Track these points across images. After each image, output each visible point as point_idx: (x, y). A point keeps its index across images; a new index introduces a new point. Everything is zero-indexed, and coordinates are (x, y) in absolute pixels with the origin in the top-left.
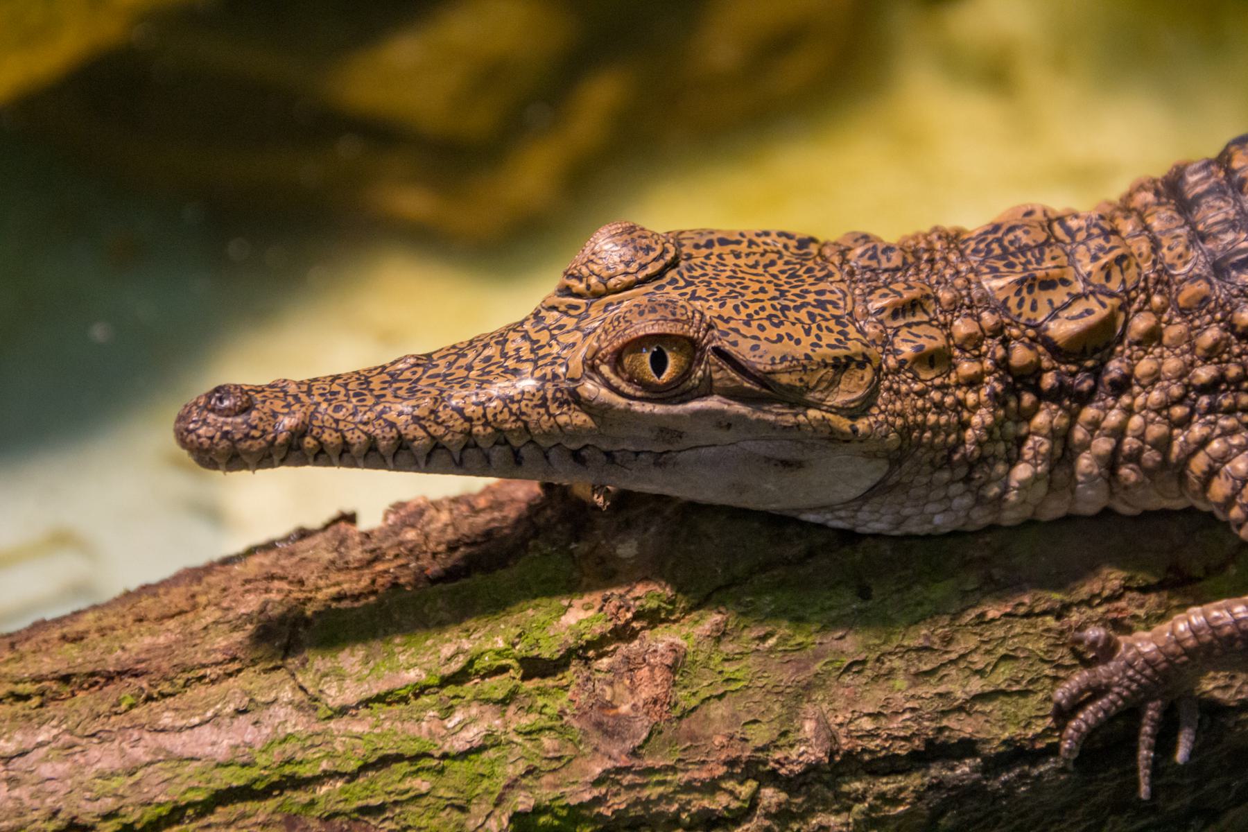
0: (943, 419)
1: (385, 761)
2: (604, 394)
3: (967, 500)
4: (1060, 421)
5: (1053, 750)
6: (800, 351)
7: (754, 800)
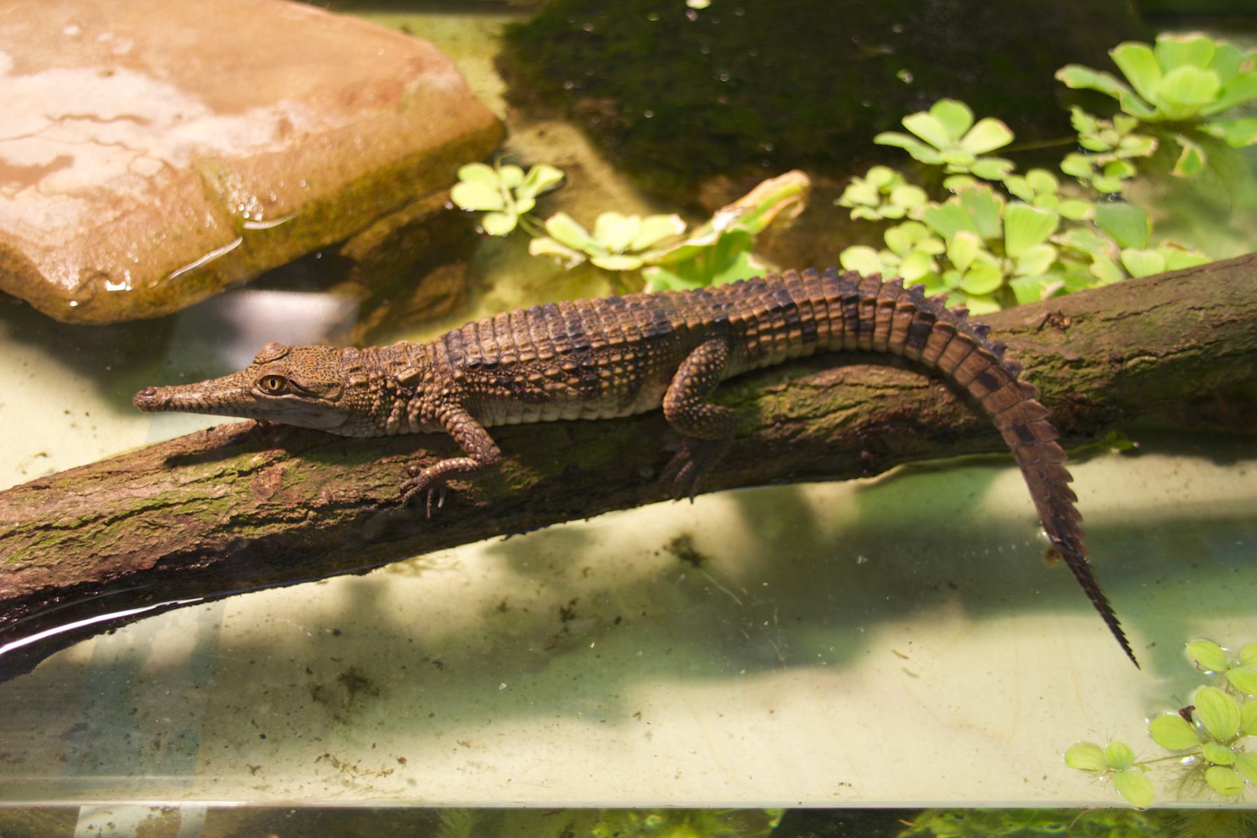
0: (364, 403)
1: (195, 500)
2: (258, 392)
3: (374, 428)
4: (403, 405)
5: (400, 502)
6: (317, 381)
7: (306, 514)
